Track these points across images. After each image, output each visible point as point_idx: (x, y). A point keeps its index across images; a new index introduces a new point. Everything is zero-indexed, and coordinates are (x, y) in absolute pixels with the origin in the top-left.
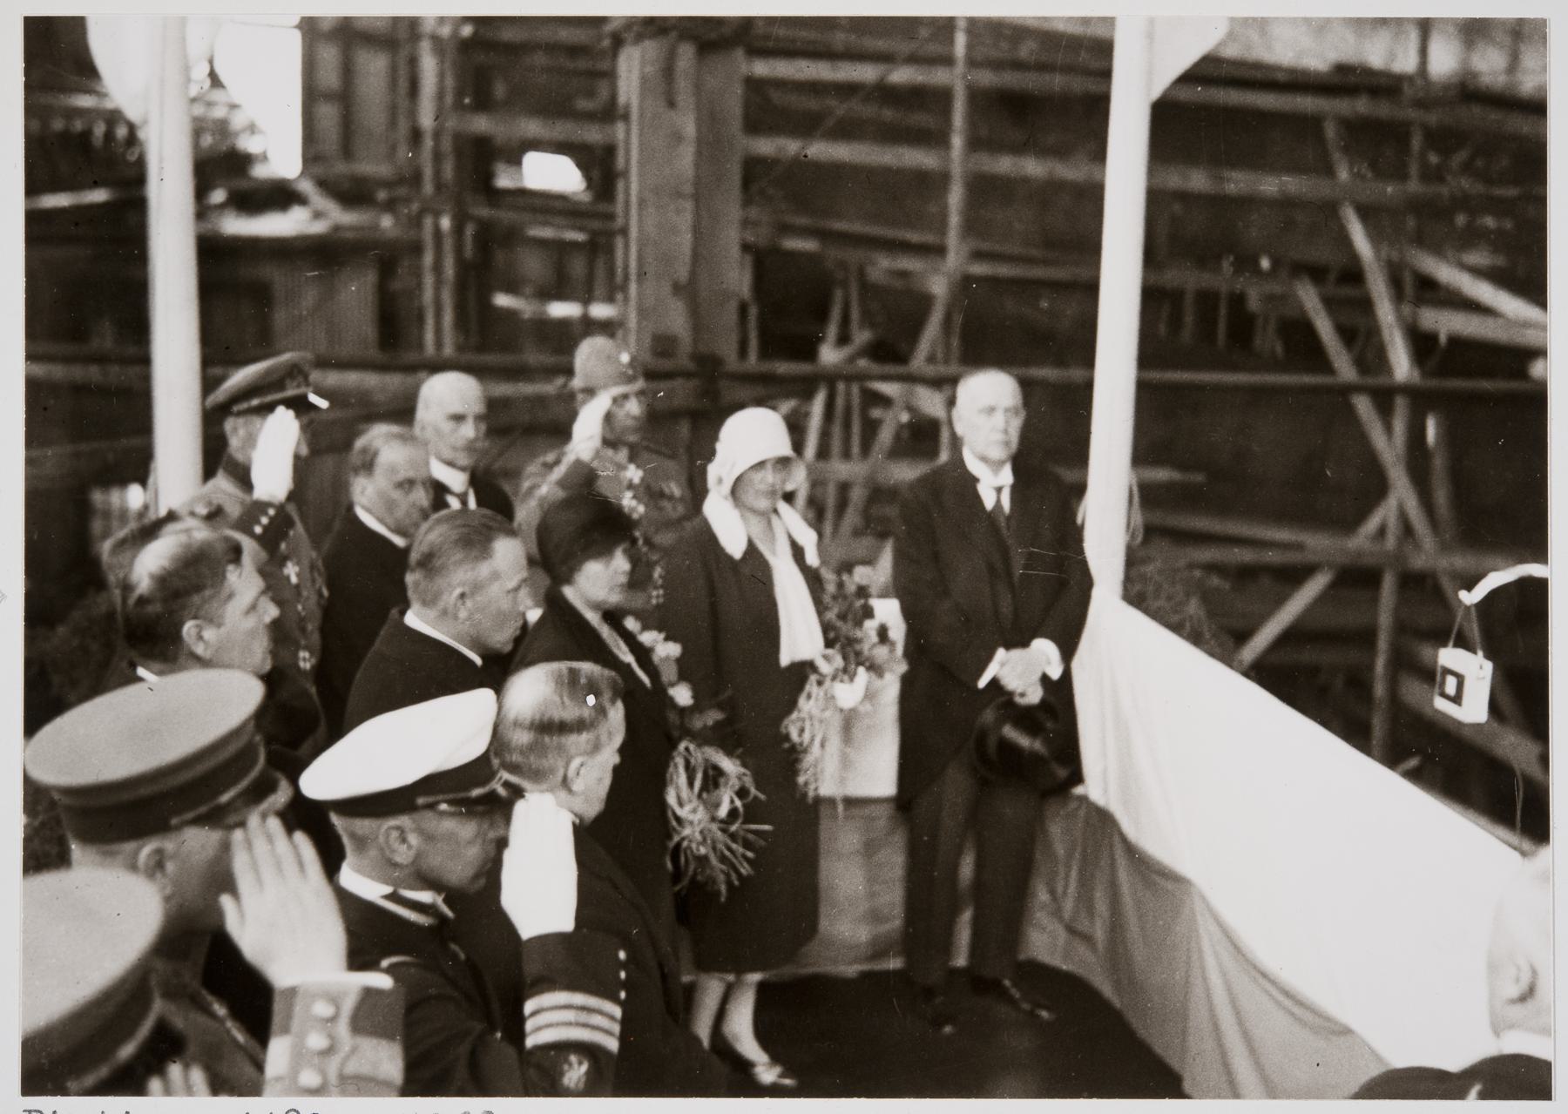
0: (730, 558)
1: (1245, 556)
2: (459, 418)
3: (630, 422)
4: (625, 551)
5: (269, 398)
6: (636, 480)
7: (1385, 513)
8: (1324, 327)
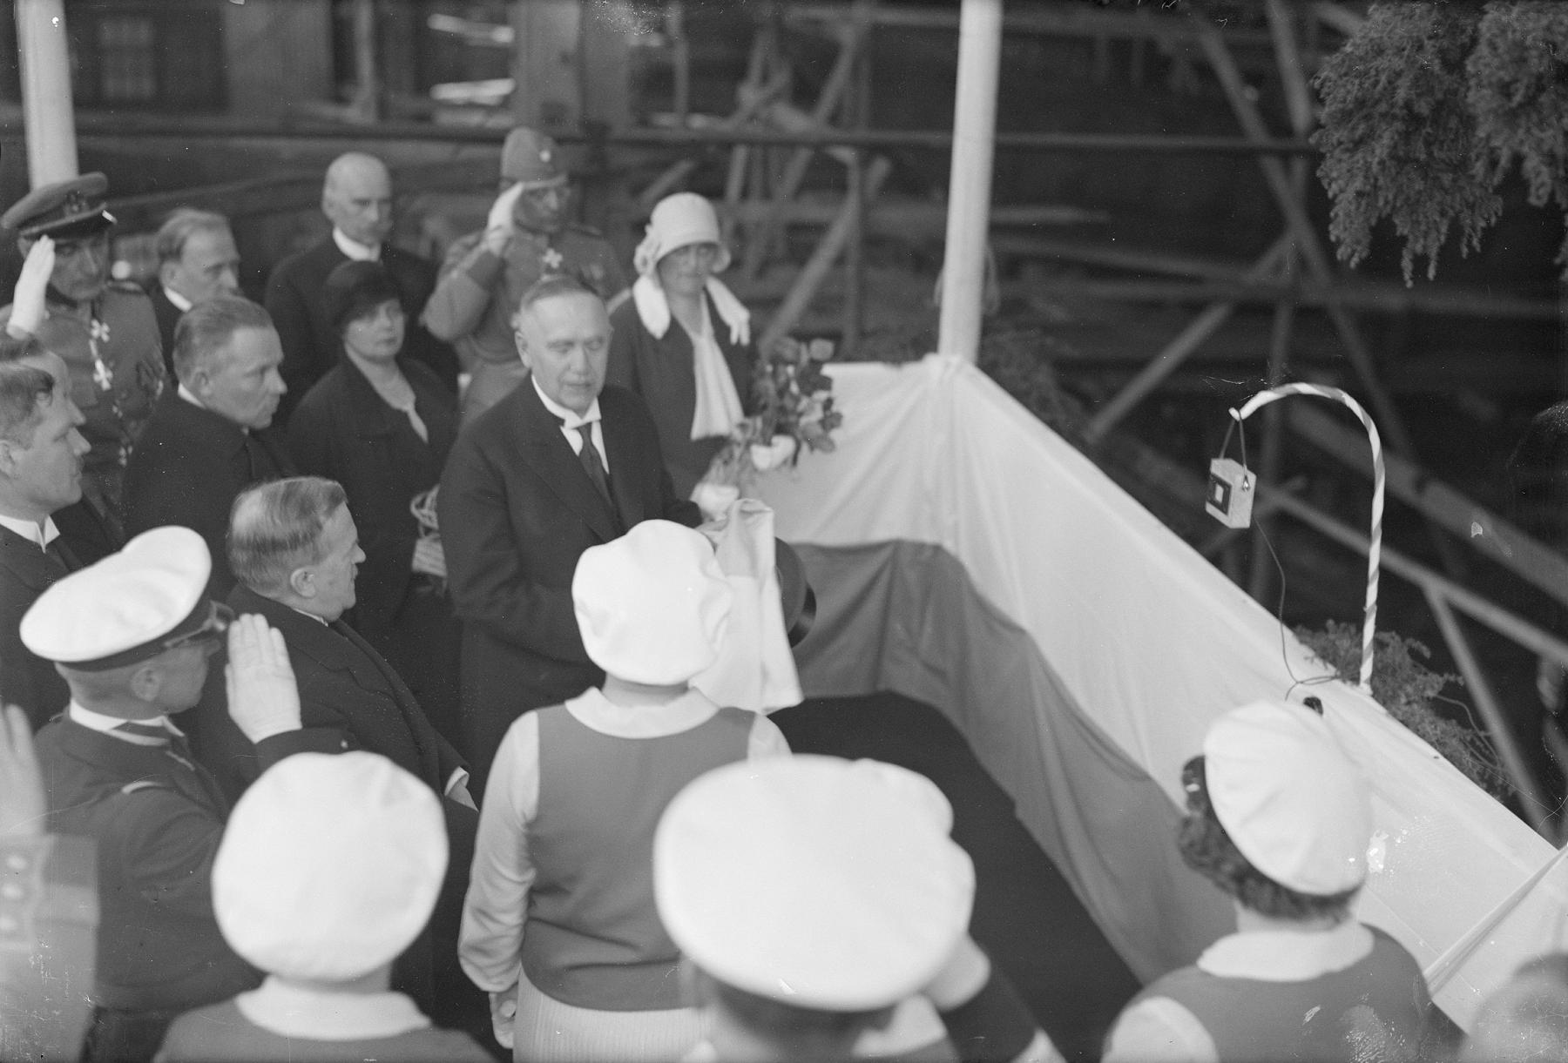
0: (652, 337)
1: (1145, 290)
2: (363, 203)
3: (545, 214)
4: (438, 579)
5: (35, 230)
6: (555, 265)
7: (1284, 250)
8: (1227, 73)
